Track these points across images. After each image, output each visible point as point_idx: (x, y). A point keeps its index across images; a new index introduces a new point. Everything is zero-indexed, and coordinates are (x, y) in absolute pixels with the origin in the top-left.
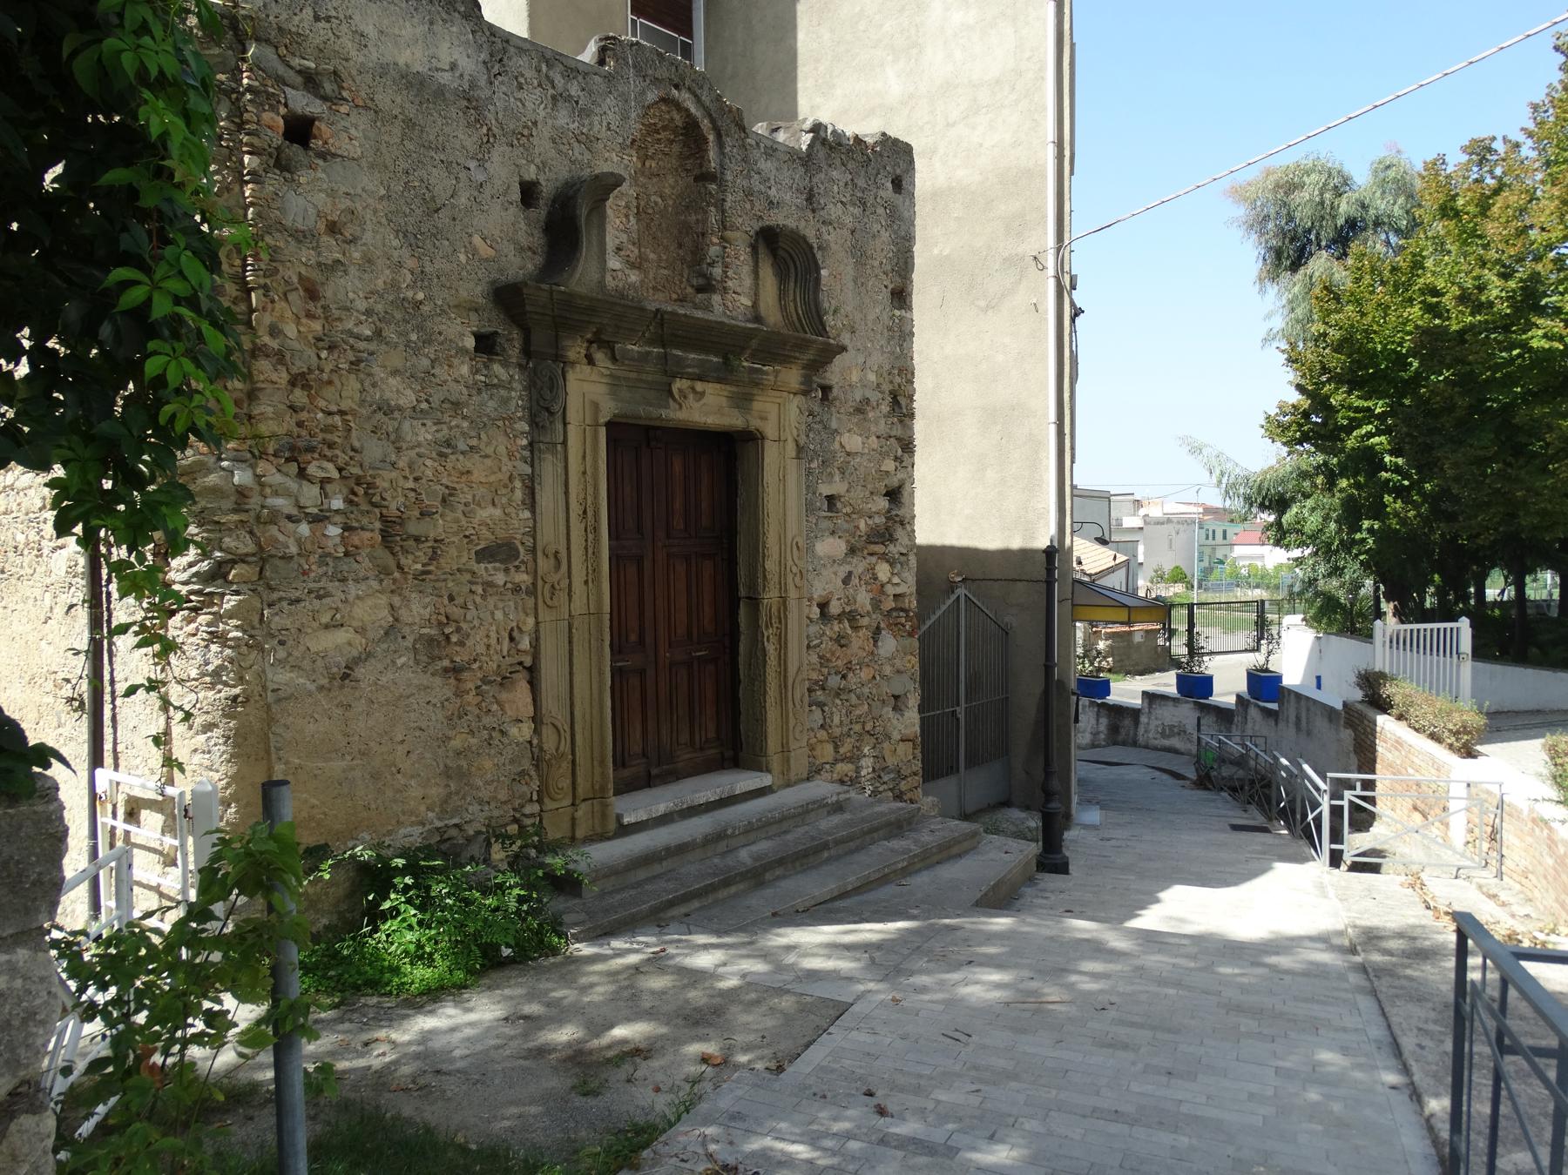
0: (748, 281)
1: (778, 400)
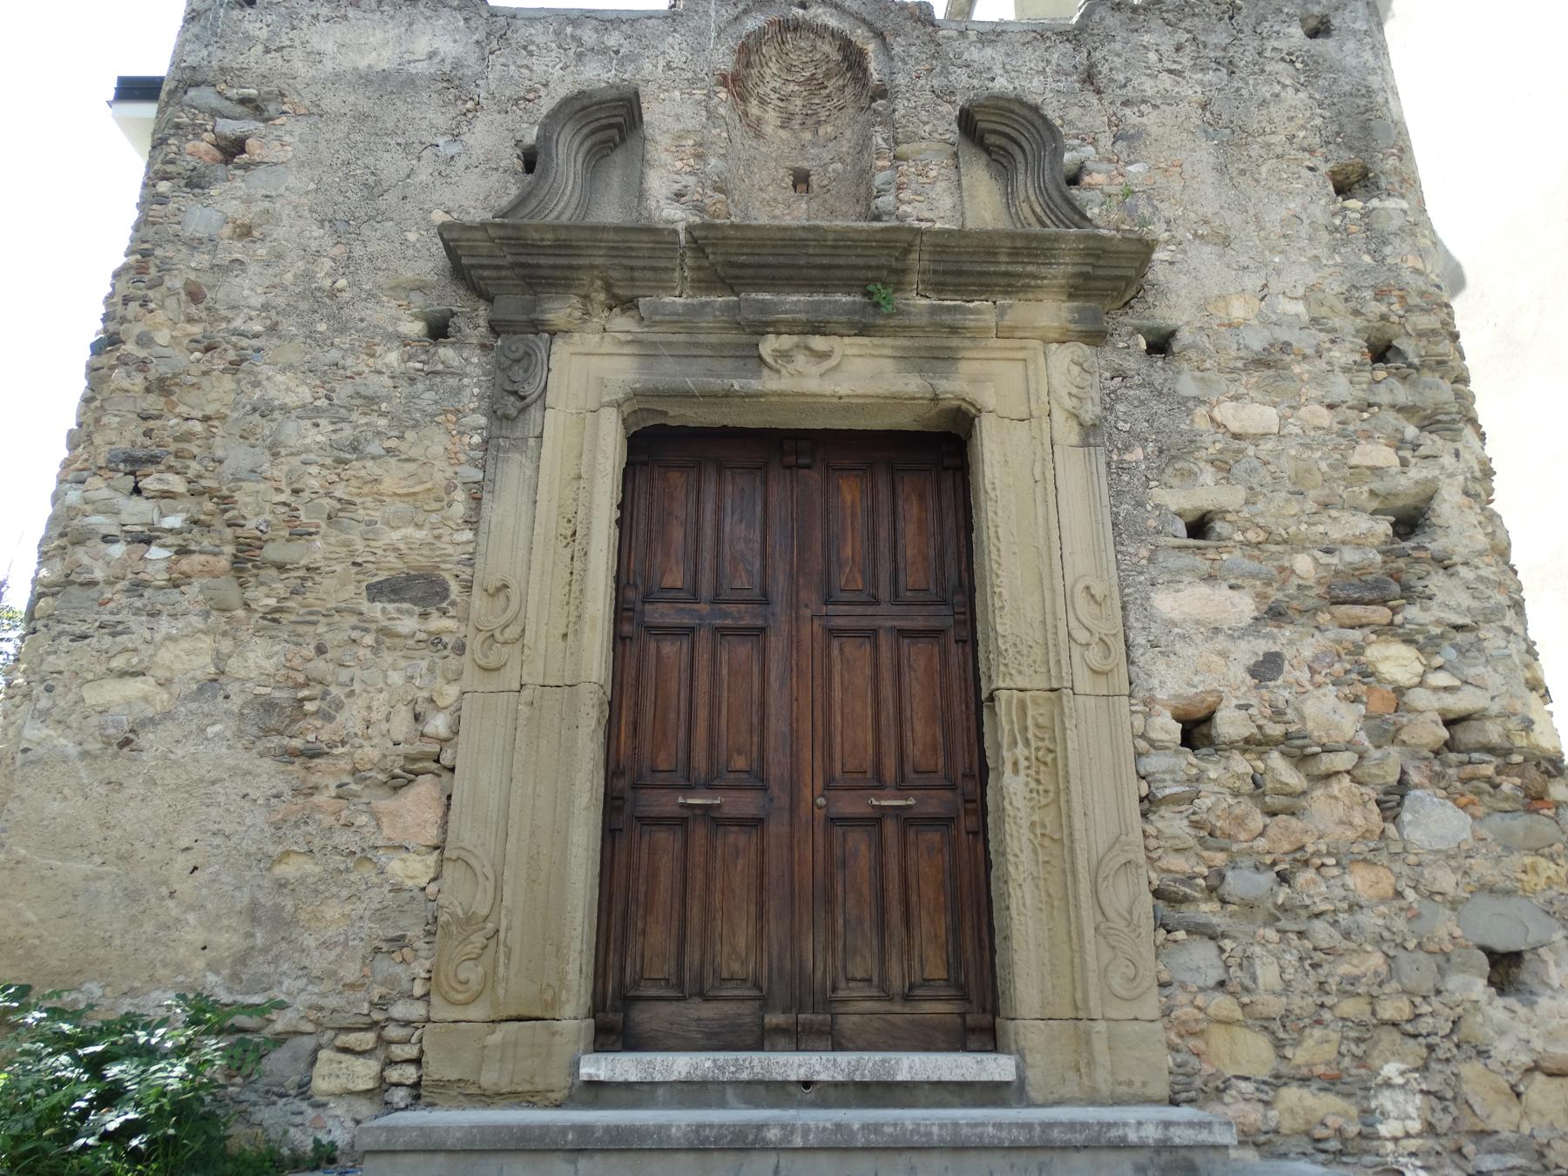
1: (1020, 355)
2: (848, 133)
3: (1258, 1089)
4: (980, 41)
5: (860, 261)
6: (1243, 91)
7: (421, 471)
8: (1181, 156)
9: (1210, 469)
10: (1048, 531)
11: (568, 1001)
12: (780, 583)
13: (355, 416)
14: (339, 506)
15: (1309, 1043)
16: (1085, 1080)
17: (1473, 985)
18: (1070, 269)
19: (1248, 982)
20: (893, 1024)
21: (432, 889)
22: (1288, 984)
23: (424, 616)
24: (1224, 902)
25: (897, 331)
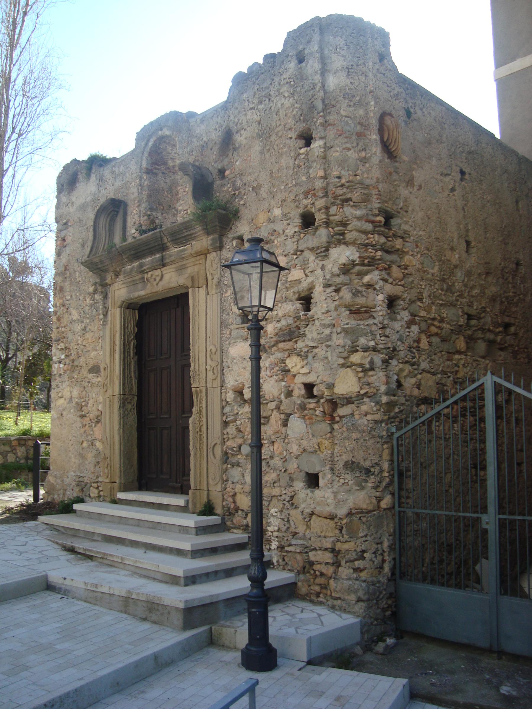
17: (299, 485)
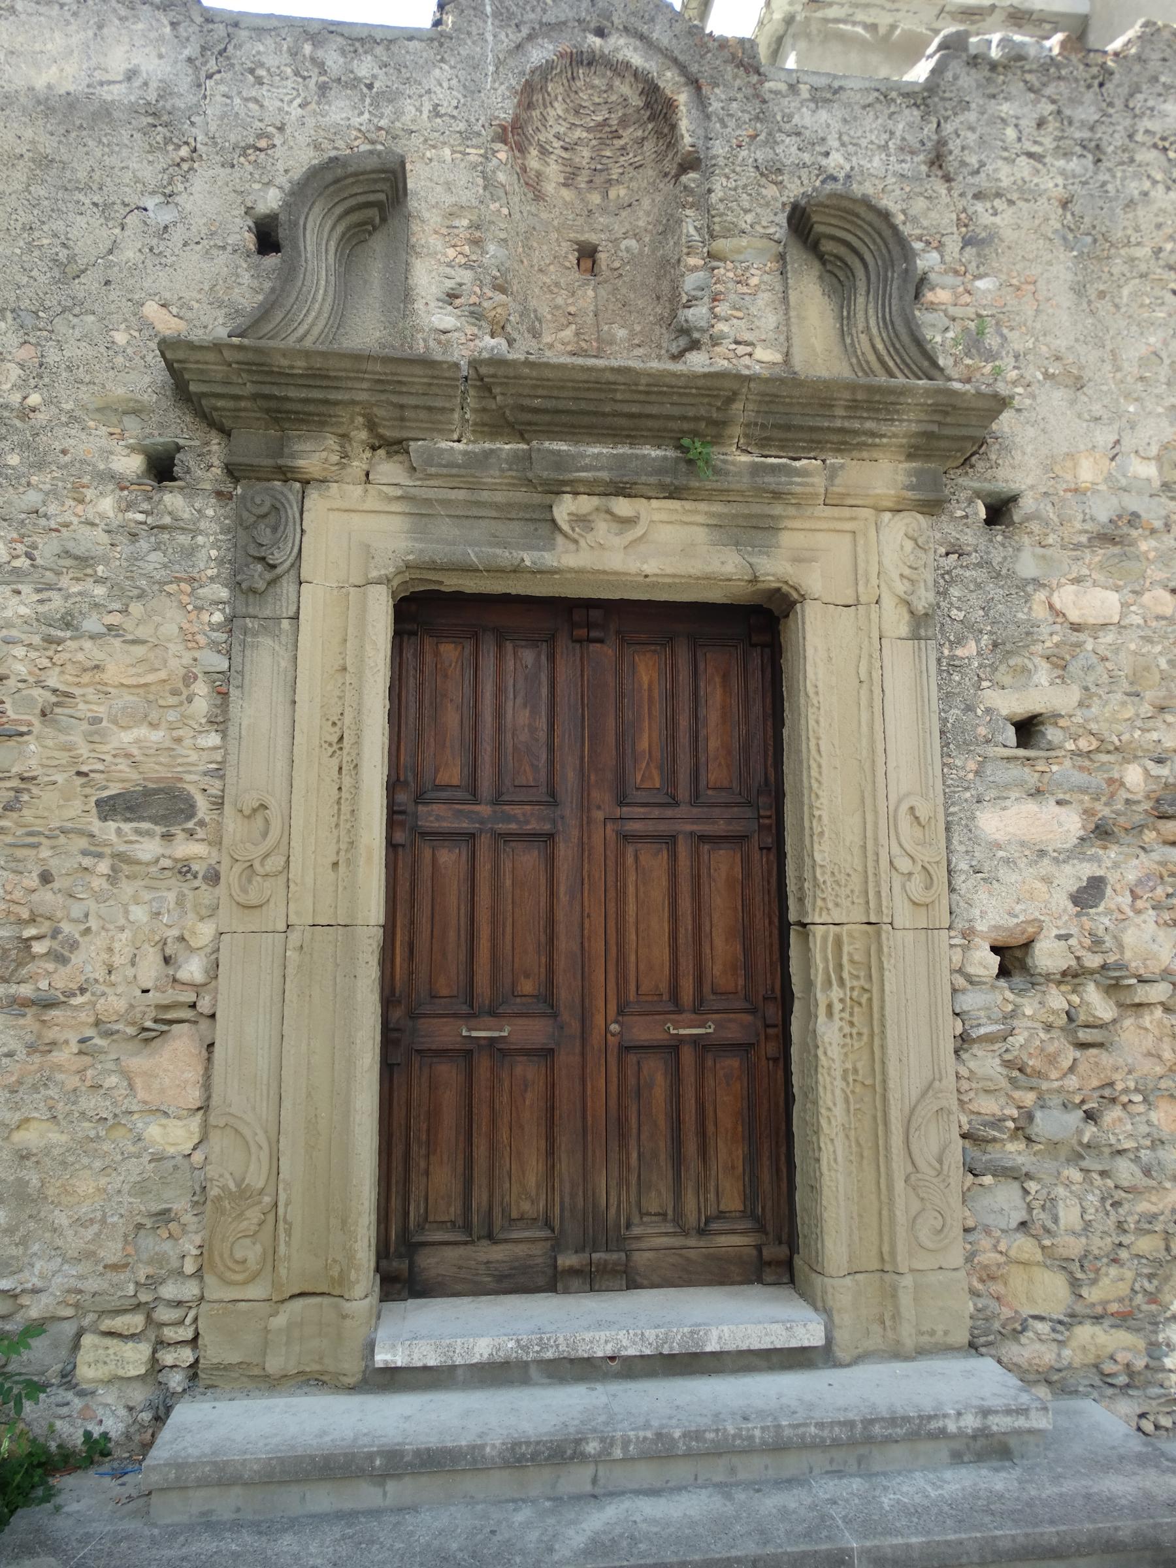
0: (770, 320)
1: (848, 526)
2: (646, 203)
3: (1054, 1330)
4: (813, 99)
5: (676, 411)
6: (1110, 187)
7: (151, 655)
8: (1035, 270)
9: (1045, 665)
10: (872, 741)
11: (358, 1282)
12: (569, 779)
13: (64, 582)
14: (54, 699)
15: (1105, 1282)
16: (890, 1334)
18: (914, 427)
19: (1050, 1224)
20: (688, 1259)
21: (198, 1157)
22: (1088, 1225)
23: (167, 837)
24: (1029, 1139)
25: (708, 496)
